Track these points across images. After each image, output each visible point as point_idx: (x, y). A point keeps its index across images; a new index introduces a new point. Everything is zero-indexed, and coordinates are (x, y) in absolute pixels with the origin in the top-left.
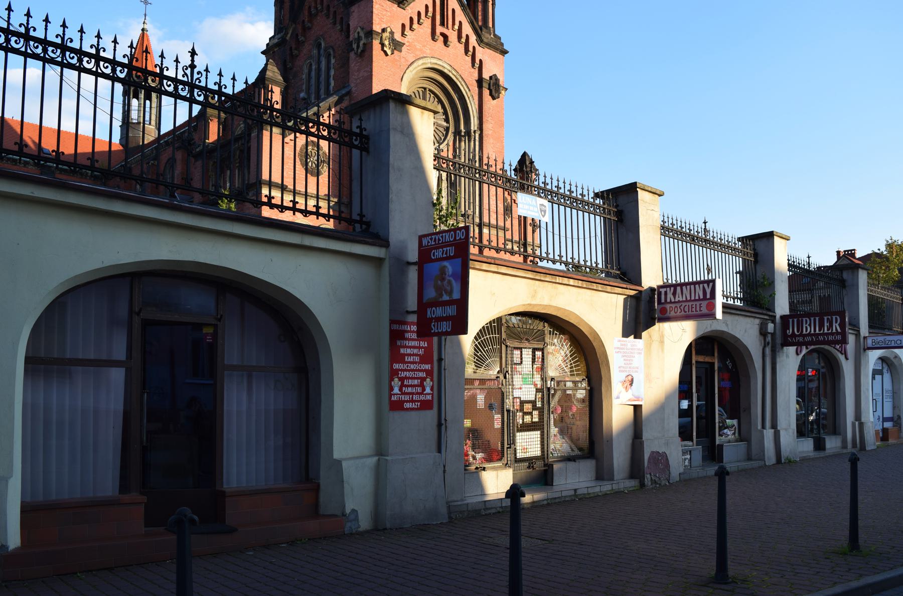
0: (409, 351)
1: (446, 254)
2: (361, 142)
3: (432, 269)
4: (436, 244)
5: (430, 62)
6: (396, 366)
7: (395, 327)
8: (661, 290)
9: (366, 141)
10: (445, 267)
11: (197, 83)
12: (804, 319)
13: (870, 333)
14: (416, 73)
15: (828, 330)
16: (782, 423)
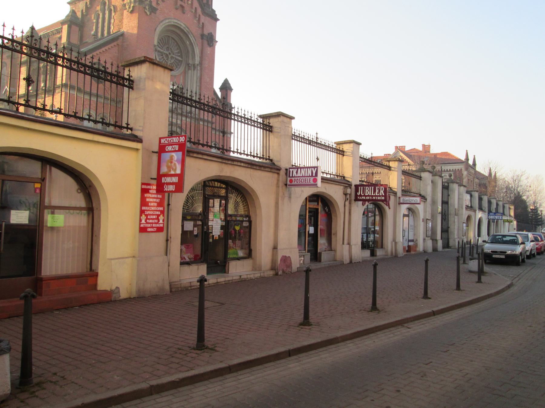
0: (151, 200)
1: (174, 149)
2: (129, 83)
3: (165, 156)
4: (168, 143)
5: (174, 21)
6: (144, 208)
7: (144, 187)
8: (290, 170)
9: (132, 83)
10: (173, 156)
11: (34, 46)
12: (366, 188)
13: (402, 195)
14: (164, 27)
15: (378, 194)
16: (353, 242)
